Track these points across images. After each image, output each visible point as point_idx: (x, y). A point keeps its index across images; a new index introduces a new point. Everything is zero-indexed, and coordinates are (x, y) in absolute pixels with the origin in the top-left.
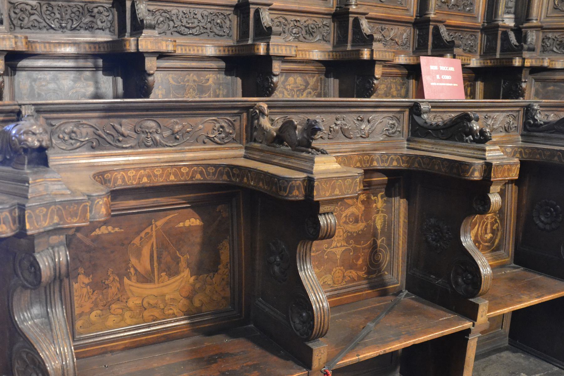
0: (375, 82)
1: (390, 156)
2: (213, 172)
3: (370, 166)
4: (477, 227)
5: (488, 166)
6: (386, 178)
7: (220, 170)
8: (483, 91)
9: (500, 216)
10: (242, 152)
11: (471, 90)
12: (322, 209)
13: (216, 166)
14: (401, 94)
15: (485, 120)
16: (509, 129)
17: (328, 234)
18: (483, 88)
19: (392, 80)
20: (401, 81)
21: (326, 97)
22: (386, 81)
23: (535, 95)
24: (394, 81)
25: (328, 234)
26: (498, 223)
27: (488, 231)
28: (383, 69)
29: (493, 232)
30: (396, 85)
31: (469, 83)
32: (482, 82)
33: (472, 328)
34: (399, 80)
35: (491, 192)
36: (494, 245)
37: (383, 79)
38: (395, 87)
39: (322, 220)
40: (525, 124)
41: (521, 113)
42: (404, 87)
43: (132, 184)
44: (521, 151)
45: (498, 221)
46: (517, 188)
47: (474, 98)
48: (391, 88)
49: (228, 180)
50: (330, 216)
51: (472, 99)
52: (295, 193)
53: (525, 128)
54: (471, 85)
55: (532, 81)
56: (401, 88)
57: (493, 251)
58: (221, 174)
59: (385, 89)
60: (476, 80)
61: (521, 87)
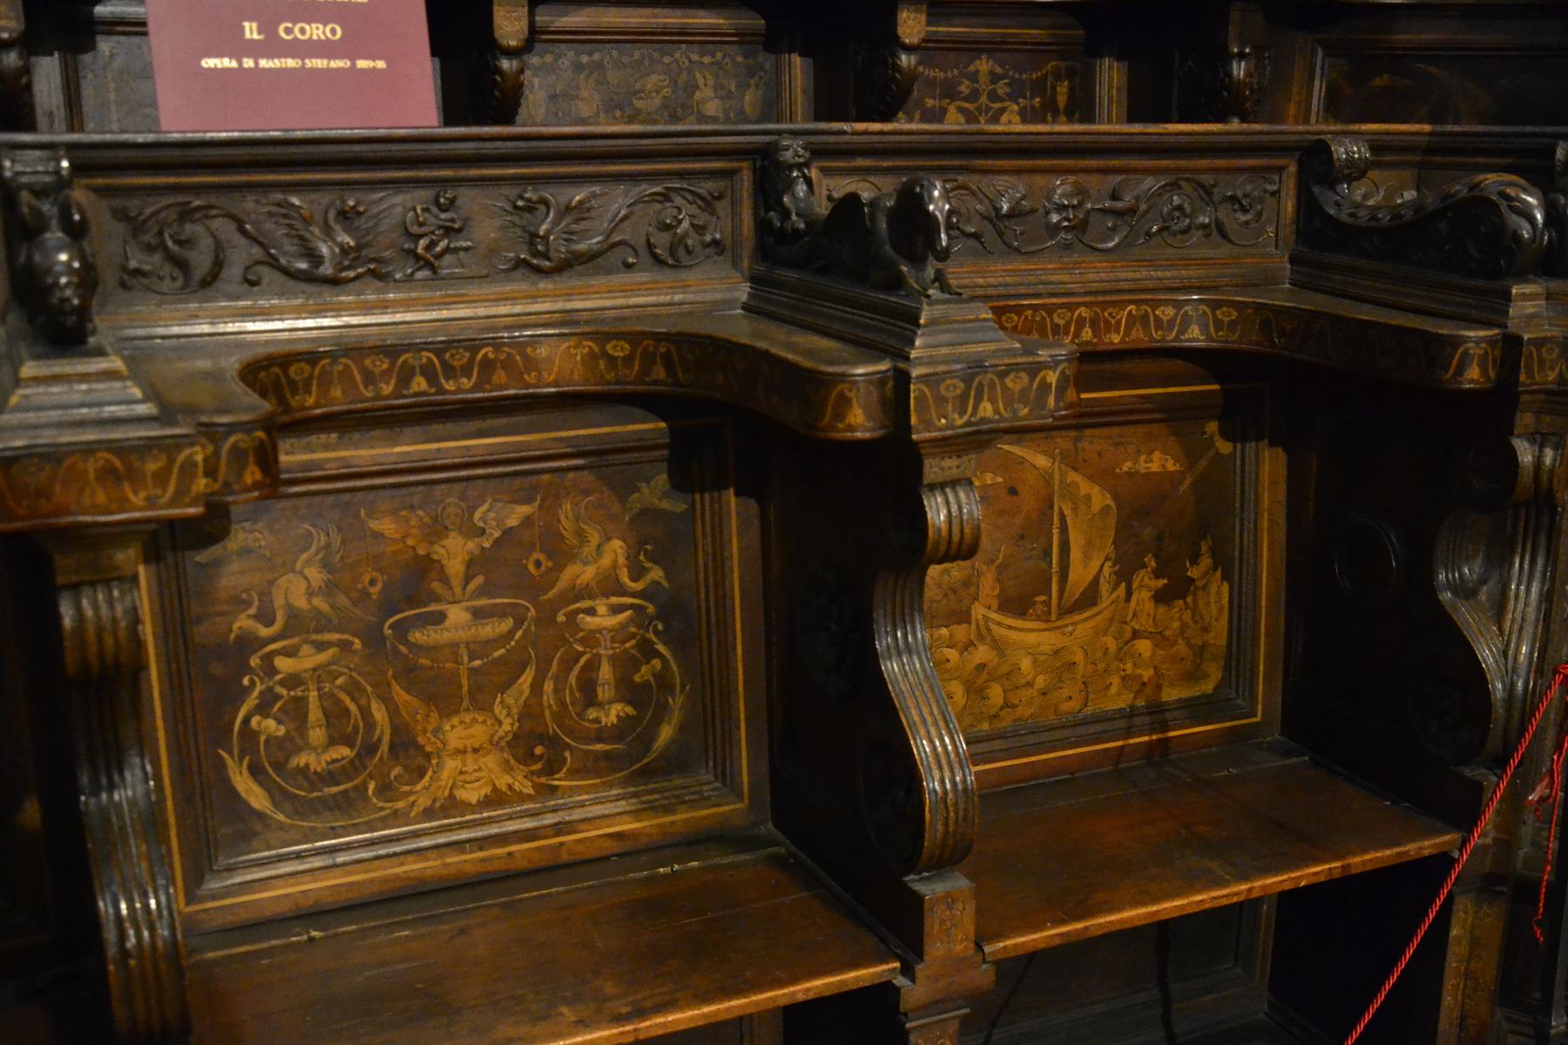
0: (505, 64)
1: (478, 348)
2: (625, 358)
3: (1177, 339)
4: (527, 678)
5: (1512, 343)
6: (663, 425)
7: (646, 348)
8: (1124, 93)
9: (666, 627)
10: (743, 292)
11: (1071, 90)
12: (934, 469)
13: (634, 338)
14: (741, 111)
15: (516, 219)
16: (681, 252)
17: (954, 545)
18: (1125, 80)
19: (695, 57)
20: (739, 59)
21: (782, 122)
22: (667, 60)
23: (1327, 110)
24: (706, 59)
25: (954, 545)
26: (659, 655)
27: (604, 693)
28: (929, 24)
29: (629, 691)
30: (716, 76)
31: (1062, 65)
32: (1119, 59)
33: (900, 981)
34: (735, 57)
35: (1516, 432)
36: (648, 750)
37: (656, 55)
38: (711, 82)
39: (938, 511)
40: (762, 226)
41: (746, 180)
42: (752, 82)
43: (1112, 343)
44: (668, 353)
45: (661, 648)
46: (753, 506)
47: (1089, 118)
48: (692, 87)
49: (670, 381)
50: (962, 495)
51: (1081, 121)
52: (1474, 372)
53: (764, 252)
54: (1071, 74)
55: (1313, 53)
56: (744, 86)
57: (647, 773)
58: (649, 358)
59: (666, 92)
60: (1094, 50)
61: (1229, 75)
